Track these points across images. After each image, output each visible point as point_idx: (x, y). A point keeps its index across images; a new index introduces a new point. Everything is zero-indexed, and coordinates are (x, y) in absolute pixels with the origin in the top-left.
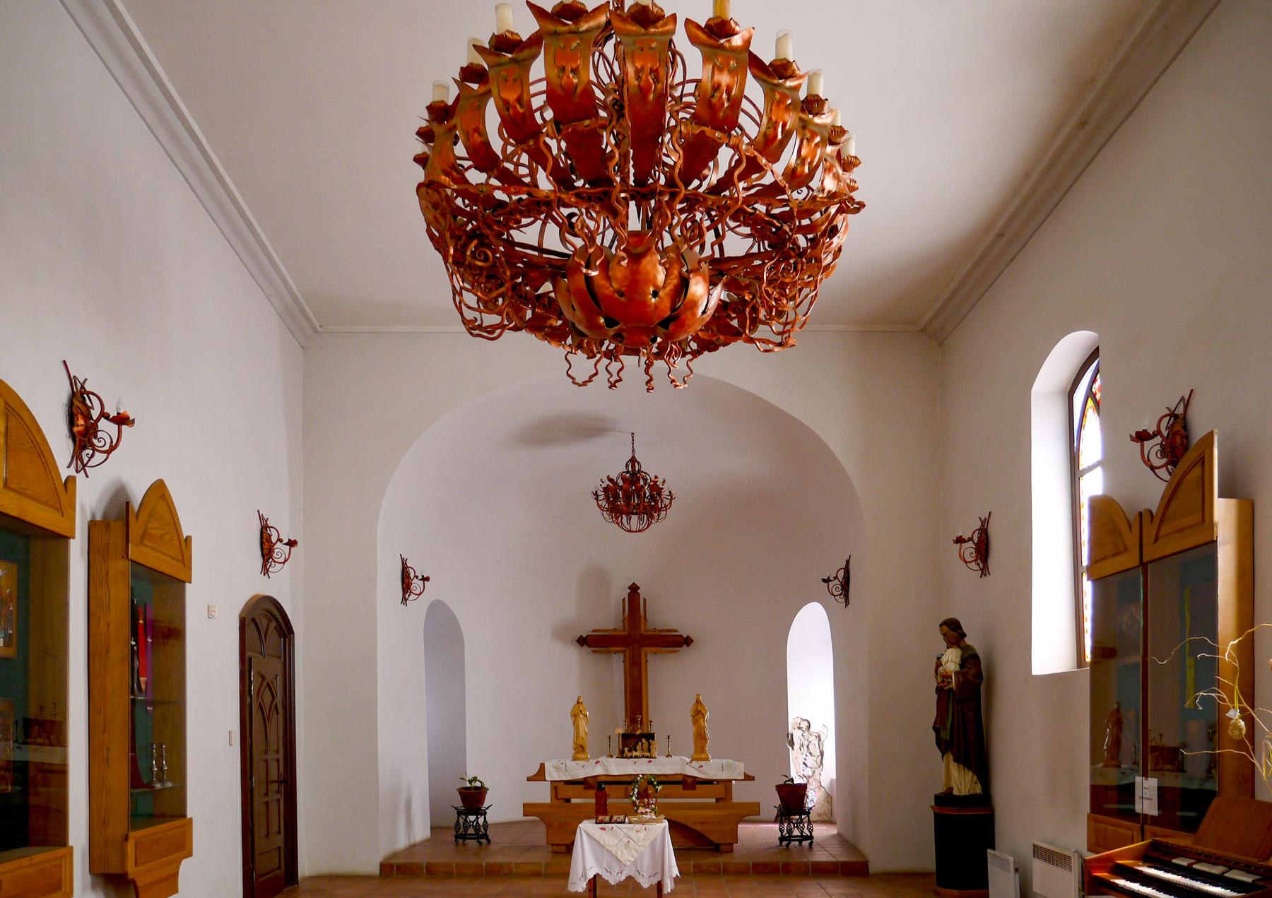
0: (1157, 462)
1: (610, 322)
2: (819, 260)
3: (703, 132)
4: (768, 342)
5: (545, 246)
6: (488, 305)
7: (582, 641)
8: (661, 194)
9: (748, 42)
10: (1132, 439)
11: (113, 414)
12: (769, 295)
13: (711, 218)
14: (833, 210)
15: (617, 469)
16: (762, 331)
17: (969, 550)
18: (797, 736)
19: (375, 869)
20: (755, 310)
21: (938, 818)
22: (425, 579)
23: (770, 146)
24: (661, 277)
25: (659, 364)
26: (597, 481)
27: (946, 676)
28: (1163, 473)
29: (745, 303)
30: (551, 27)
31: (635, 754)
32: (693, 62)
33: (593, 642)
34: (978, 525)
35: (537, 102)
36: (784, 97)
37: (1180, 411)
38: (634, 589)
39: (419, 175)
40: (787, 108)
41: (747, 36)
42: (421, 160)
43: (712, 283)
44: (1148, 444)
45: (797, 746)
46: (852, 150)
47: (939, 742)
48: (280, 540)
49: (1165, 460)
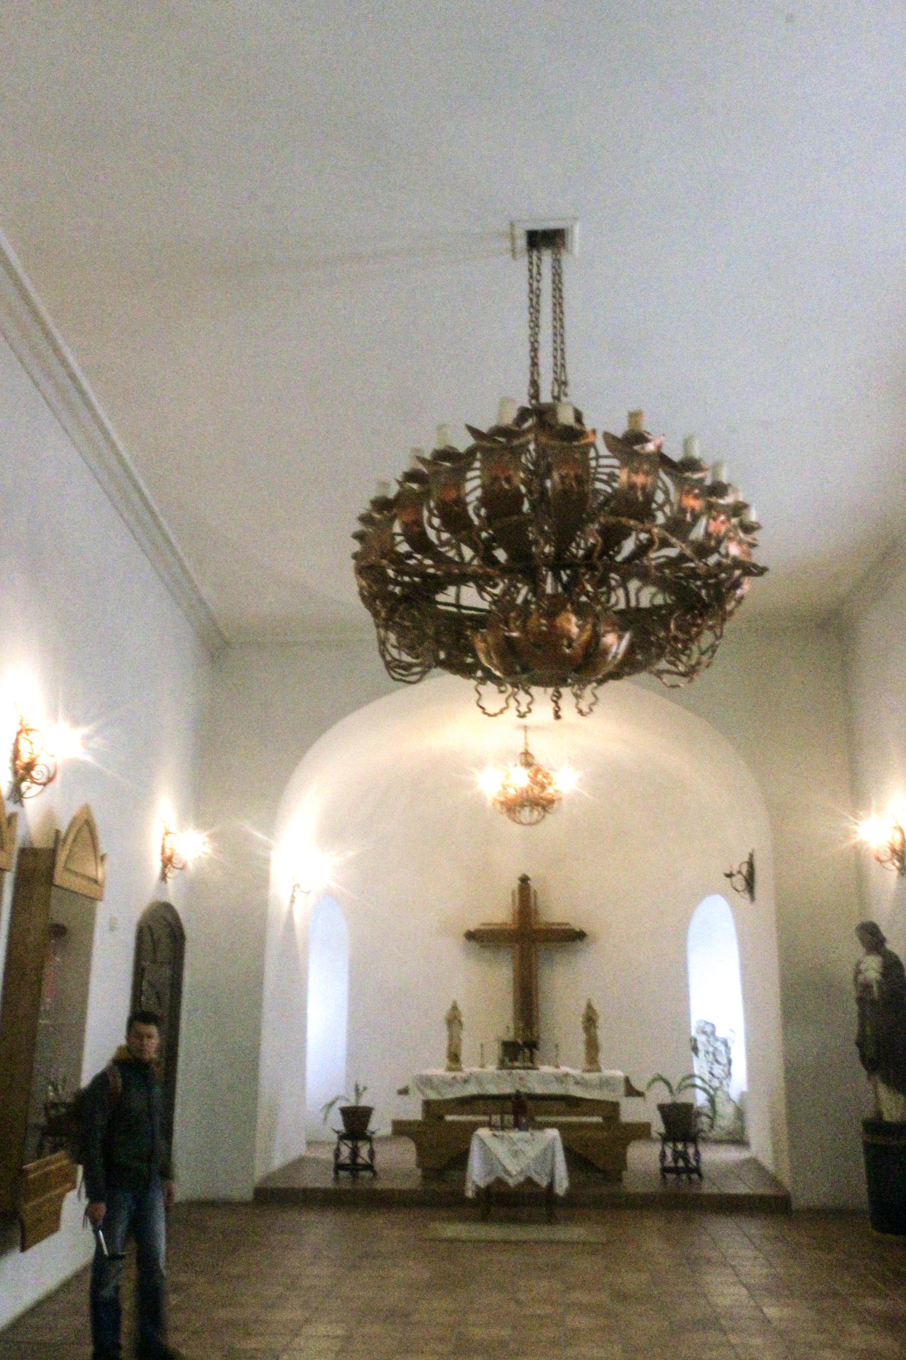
3: (620, 522)
6: (411, 649)
7: (471, 936)
8: (579, 566)
9: (659, 447)
16: (663, 665)
18: (701, 1039)
19: (249, 1196)
21: (868, 1147)
24: (575, 630)
25: (566, 691)
27: (866, 987)
30: (487, 444)
31: (517, 1064)
32: (604, 461)
33: (481, 938)
38: (524, 880)
39: (356, 546)
41: (658, 442)
45: (701, 1054)
46: (753, 516)
47: (863, 1058)
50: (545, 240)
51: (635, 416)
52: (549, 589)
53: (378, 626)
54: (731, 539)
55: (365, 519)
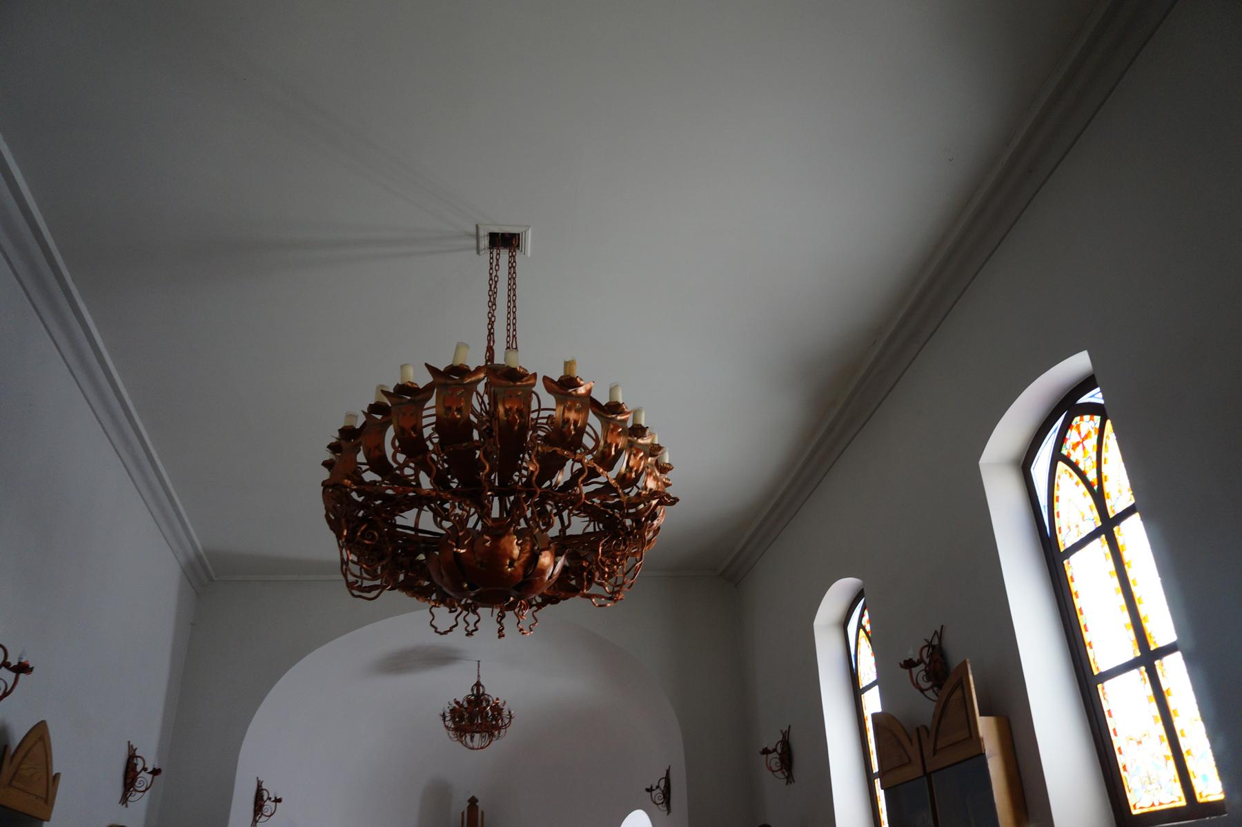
0: (925, 685)
1: (471, 588)
2: (642, 537)
4: (601, 597)
5: (421, 527)
8: (520, 492)
9: (589, 391)
10: (902, 666)
11: (14, 663)
12: (603, 563)
13: (557, 507)
14: (654, 502)
15: (462, 692)
16: (594, 589)
17: (774, 759)
20: (591, 573)
22: (278, 801)
23: (607, 461)
24: (516, 551)
25: (510, 615)
26: (445, 705)
28: (930, 693)
29: (584, 569)
30: (442, 381)
32: (545, 402)
34: (781, 738)
35: (427, 432)
36: (617, 427)
37: (936, 642)
38: (473, 801)
39: (325, 474)
40: (619, 434)
41: (588, 387)
42: (327, 464)
43: (557, 554)
44: (915, 670)
48: (145, 769)
49: (930, 684)
50: (505, 241)
51: (568, 365)
52: (495, 513)
53: (341, 548)
54: (649, 474)
55: (333, 448)
